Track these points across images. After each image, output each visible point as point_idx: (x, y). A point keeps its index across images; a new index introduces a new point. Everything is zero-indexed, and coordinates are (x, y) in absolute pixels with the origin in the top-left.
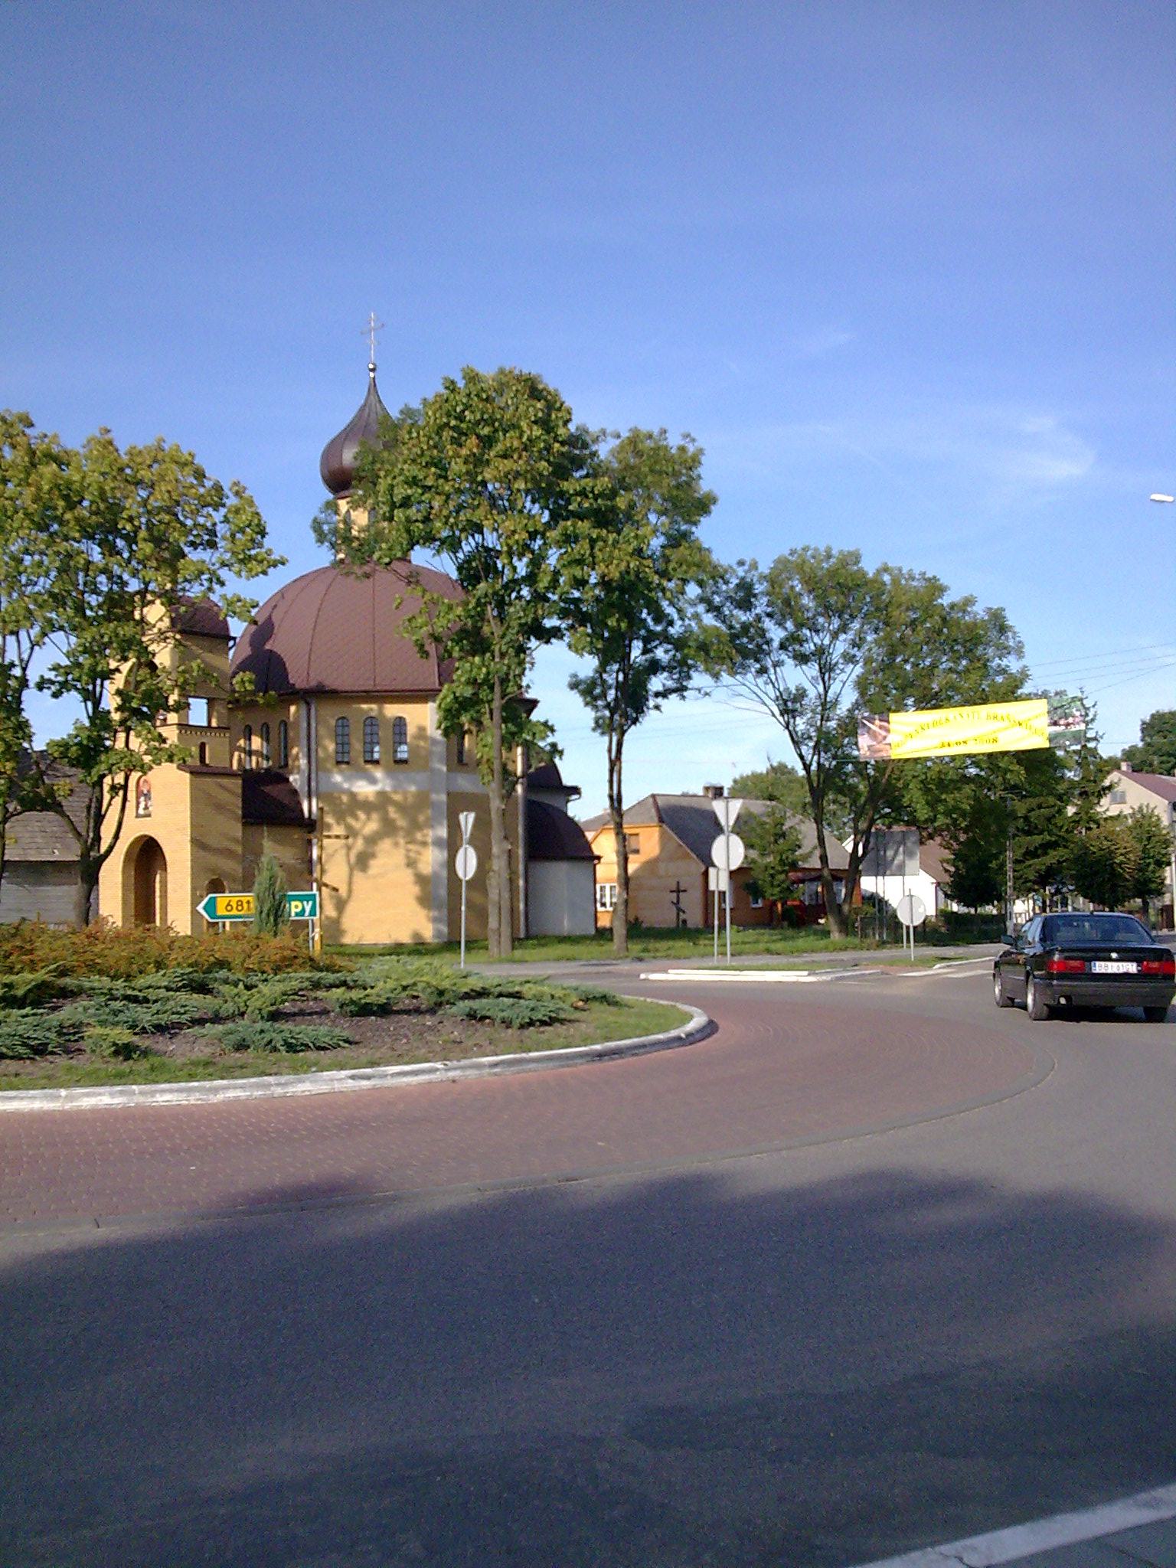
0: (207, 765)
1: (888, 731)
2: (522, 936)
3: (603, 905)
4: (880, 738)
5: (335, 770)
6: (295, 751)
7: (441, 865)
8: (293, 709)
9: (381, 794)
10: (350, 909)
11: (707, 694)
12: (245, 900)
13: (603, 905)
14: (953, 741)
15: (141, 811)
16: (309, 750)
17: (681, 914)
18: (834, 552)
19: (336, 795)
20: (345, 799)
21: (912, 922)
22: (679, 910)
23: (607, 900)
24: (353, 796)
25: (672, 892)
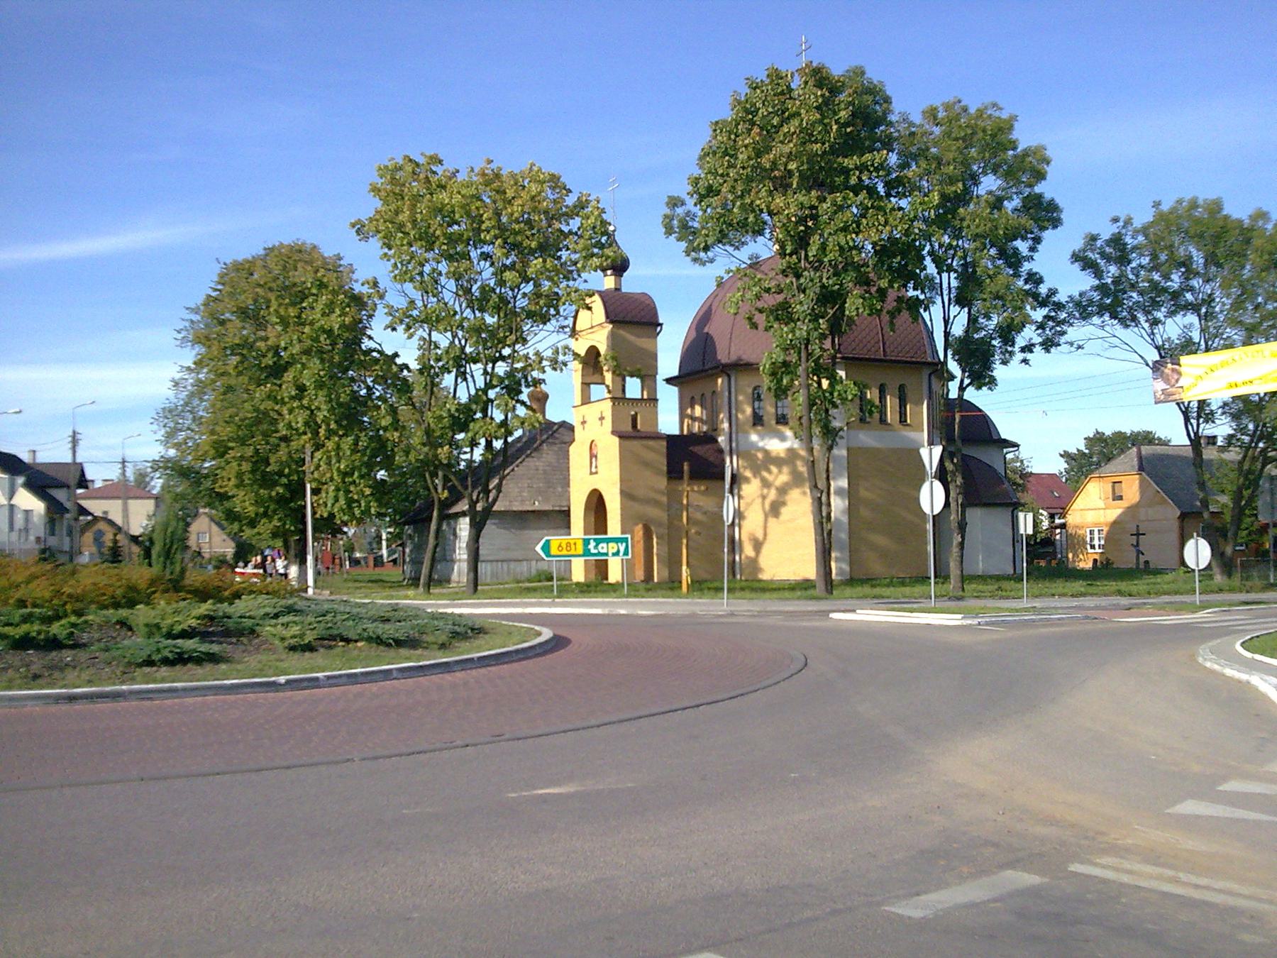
0: (639, 431)
1: (1179, 374)
2: (261, 571)
3: (1093, 547)
4: (1173, 381)
5: (752, 431)
6: (721, 416)
7: (843, 512)
8: (720, 381)
9: (791, 451)
10: (765, 550)
11: (1080, 347)
12: (572, 542)
13: (1093, 547)
14: (1239, 382)
15: (594, 470)
16: (730, 416)
17: (1141, 555)
18: (1201, 202)
19: (753, 452)
20: (760, 455)
21: (1198, 566)
22: (1139, 552)
23: (1096, 542)
24: (766, 452)
25: (1132, 535)
